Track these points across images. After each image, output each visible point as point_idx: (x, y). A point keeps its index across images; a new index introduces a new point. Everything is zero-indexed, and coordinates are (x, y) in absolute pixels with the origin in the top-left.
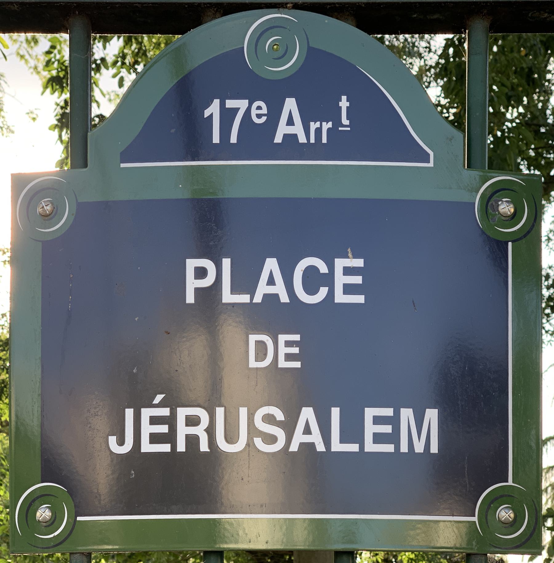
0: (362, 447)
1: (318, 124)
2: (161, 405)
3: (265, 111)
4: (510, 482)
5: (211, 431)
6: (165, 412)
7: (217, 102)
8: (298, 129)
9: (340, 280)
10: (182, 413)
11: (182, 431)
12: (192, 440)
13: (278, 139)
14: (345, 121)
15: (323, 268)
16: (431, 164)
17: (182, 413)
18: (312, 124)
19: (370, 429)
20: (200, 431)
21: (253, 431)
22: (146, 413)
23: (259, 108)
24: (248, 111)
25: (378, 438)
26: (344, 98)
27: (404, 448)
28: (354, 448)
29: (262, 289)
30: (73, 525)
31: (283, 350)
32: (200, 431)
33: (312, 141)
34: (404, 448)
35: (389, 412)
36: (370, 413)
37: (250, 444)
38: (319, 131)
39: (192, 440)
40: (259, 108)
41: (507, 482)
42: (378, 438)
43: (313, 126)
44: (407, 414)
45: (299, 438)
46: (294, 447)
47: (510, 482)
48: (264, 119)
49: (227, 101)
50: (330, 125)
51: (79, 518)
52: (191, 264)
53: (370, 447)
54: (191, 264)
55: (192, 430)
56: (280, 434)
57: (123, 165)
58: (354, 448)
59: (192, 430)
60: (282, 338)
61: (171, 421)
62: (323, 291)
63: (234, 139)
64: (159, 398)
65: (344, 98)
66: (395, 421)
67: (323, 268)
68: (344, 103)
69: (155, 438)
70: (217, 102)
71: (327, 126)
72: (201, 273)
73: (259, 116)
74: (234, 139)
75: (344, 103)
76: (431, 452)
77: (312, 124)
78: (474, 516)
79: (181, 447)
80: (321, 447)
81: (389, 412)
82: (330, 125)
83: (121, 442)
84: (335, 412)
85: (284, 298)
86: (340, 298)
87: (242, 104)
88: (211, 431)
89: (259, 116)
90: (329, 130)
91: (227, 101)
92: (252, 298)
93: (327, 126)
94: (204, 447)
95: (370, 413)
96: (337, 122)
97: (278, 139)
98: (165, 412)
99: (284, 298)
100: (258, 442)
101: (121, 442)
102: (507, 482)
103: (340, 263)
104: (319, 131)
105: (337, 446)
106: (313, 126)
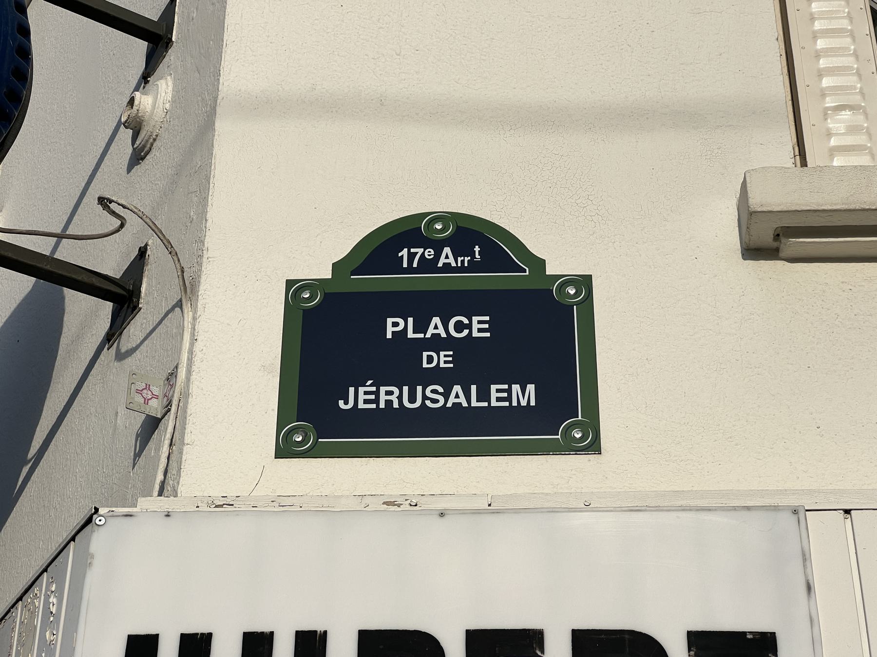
0: (489, 403)
1: (462, 258)
2: (370, 385)
3: (433, 253)
4: (580, 418)
5: (400, 398)
6: (374, 389)
7: (406, 250)
8: (451, 260)
9: (475, 326)
10: (383, 389)
11: (383, 398)
12: (389, 403)
13: (440, 265)
14: (477, 256)
15: (466, 321)
16: (527, 273)
17: (383, 389)
18: (459, 258)
19: (494, 395)
20: (394, 398)
21: (425, 397)
22: (361, 390)
23: (429, 252)
24: (423, 253)
25: (499, 399)
26: (477, 247)
27: (515, 404)
28: (485, 404)
29: (431, 331)
30: (316, 442)
31: (442, 359)
32: (394, 398)
33: (459, 265)
34: (515, 404)
35: (506, 387)
36: (494, 388)
37: (423, 402)
38: (463, 262)
39: (389, 403)
40: (429, 252)
41: (578, 418)
42: (499, 399)
43: (460, 259)
44: (516, 388)
45: (452, 400)
46: (449, 405)
47: (580, 418)
48: (432, 256)
49: (487, 405)
50: (469, 258)
51: (319, 440)
52: (390, 321)
53: (494, 403)
54: (390, 321)
55: (389, 398)
56: (442, 399)
57: (352, 277)
58: (485, 404)
59: (389, 398)
60: (442, 354)
61: (377, 393)
62: (466, 332)
63: (415, 265)
64: (369, 382)
65: (477, 247)
66: (509, 391)
67: (466, 321)
68: (477, 249)
69: (366, 402)
70: (406, 250)
71: (467, 259)
72: (395, 324)
73: (429, 255)
74: (415, 265)
75: (477, 249)
76: (388, 319)
77: (459, 258)
78: (558, 435)
79: (382, 405)
80: (465, 404)
81: (506, 387)
82: (469, 258)
83: (346, 403)
84: (474, 388)
85: (444, 335)
86: (475, 334)
87: (420, 251)
88: (400, 398)
89: (429, 255)
90: (468, 260)
91: (487, 405)
92: (425, 336)
93: (467, 259)
94: (396, 405)
95: (494, 388)
96: (473, 256)
97: (440, 265)
98: (374, 389)
99: (444, 335)
100: (428, 403)
101: (346, 403)
102: (578, 418)
103: (475, 319)
104: (463, 262)
105: (474, 403)
106: (460, 259)
